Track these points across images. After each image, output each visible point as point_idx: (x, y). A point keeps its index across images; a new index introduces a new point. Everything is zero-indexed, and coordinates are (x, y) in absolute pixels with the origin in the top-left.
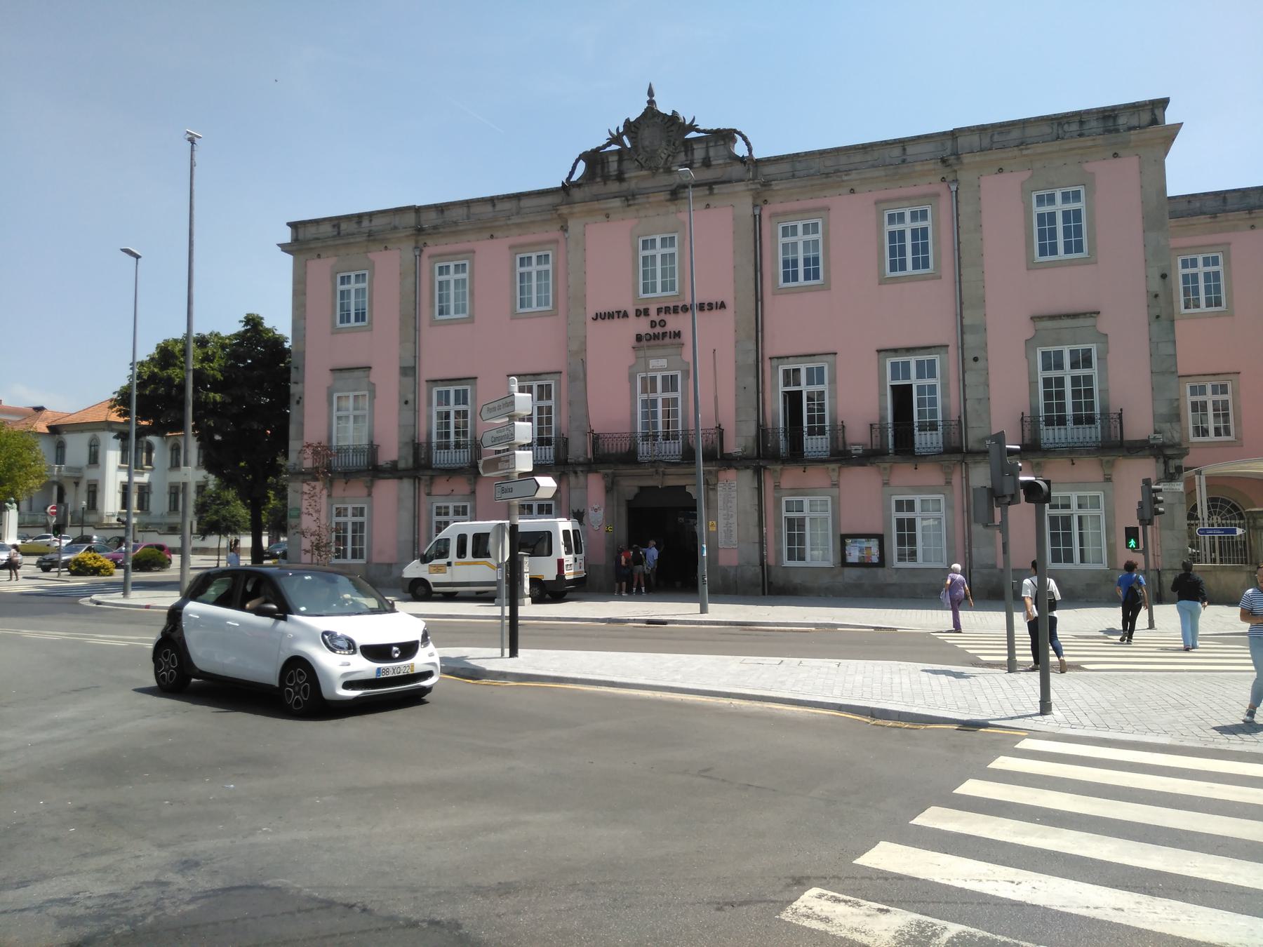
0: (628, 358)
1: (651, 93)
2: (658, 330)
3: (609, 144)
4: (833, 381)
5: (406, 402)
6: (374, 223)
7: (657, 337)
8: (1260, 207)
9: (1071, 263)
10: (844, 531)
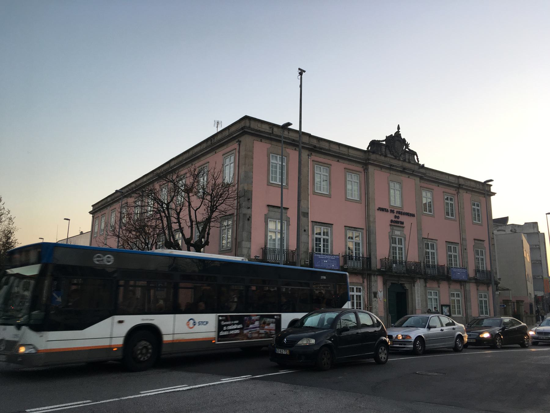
0: (388, 229)
1: (399, 128)
2: (396, 220)
4: (437, 250)
5: (305, 231)
6: (290, 134)
10: (442, 304)
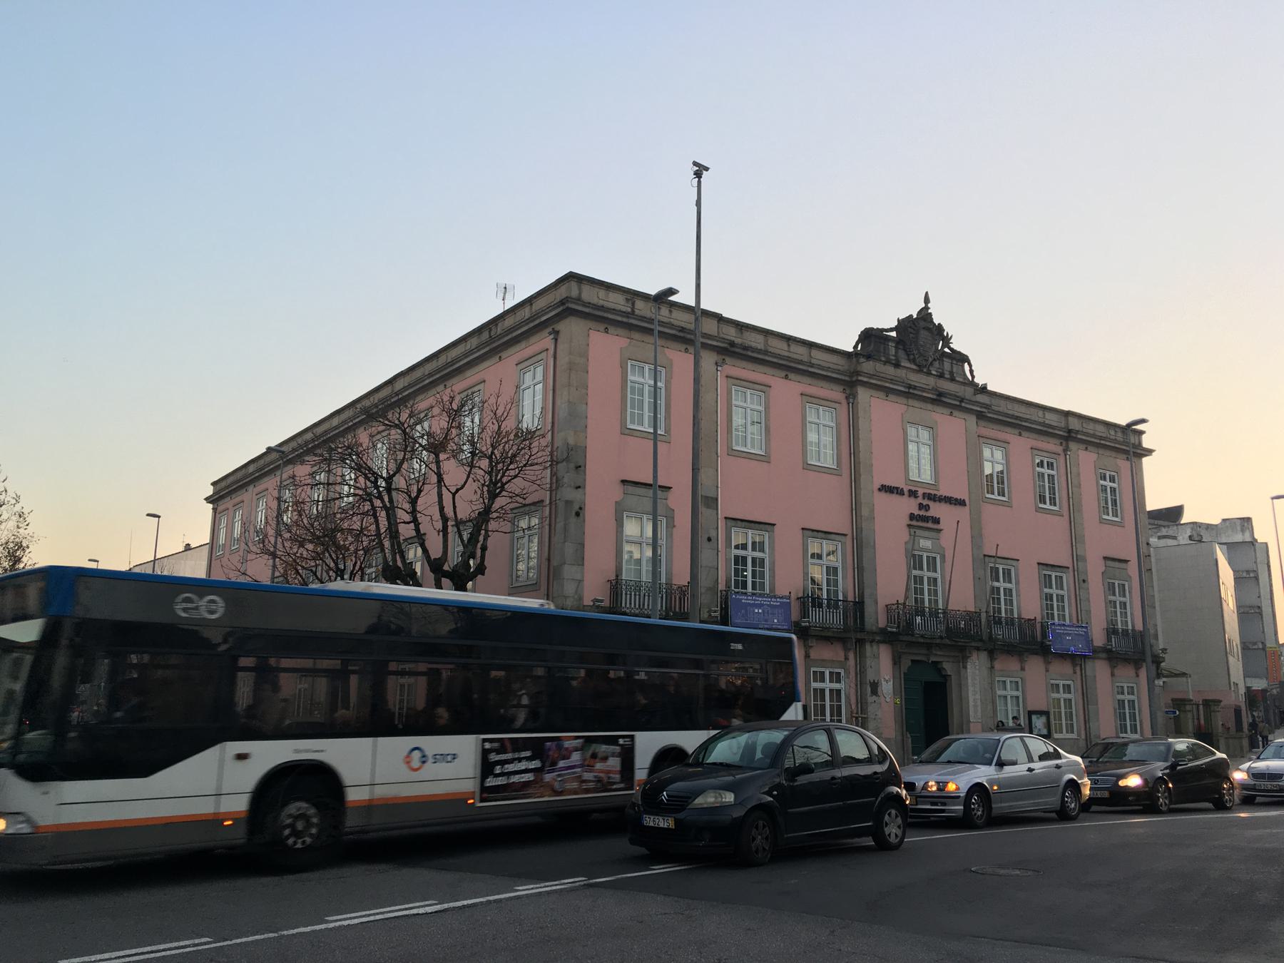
0: (904, 535)
1: (927, 300)
2: (922, 513)
3: (891, 330)
7: (922, 522)
8: (113, 660)
9: (772, 548)
